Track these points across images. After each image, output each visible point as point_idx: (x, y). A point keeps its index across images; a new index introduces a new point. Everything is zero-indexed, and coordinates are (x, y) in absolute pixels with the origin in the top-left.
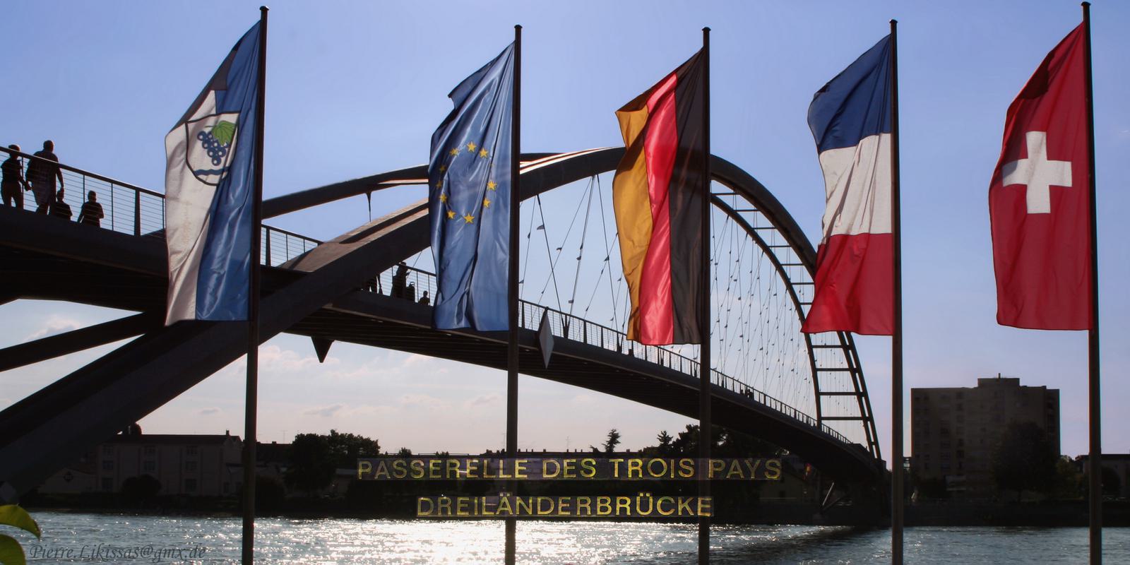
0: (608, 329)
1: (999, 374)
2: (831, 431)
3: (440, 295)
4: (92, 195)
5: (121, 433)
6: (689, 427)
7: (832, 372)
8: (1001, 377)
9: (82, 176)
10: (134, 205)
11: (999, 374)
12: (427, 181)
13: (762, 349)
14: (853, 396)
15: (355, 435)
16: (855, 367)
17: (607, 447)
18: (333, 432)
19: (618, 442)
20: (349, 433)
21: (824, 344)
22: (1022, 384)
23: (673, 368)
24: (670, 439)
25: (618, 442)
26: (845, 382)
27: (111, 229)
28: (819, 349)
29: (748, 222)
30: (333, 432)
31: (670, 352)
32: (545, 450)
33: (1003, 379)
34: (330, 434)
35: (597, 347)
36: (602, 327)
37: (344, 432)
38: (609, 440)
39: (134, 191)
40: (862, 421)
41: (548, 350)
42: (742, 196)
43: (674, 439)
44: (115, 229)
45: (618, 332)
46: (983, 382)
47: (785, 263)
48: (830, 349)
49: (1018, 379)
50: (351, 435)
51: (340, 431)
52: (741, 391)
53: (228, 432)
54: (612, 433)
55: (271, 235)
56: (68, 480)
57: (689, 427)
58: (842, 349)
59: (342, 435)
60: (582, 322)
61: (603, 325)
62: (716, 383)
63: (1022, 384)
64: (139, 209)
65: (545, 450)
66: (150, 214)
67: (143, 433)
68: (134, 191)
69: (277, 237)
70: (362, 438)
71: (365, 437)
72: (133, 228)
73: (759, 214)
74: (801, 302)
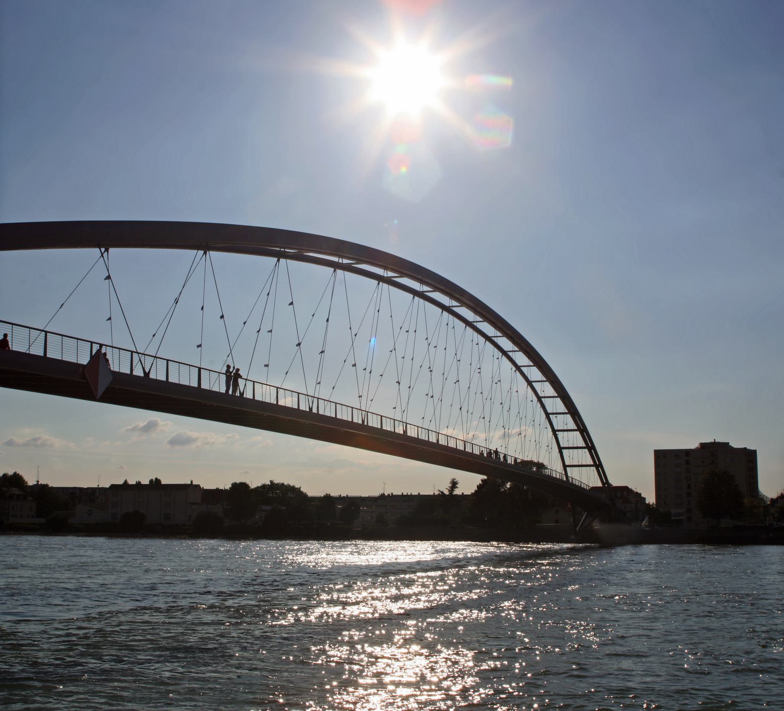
1: (715, 440)
2: (582, 484)
3: (311, 407)
4: (482, 451)
5: (508, 485)
6: (482, 480)
7: (572, 446)
8: (716, 441)
9: (178, 364)
10: (90, 350)
11: (715, 440)
12: (673, 518)
14: (592, 468)
15: (286, 484)
17: (449, 491)
18: (271, 482)
19: (457, 487)
25: (457, 487)
27: (61, 359)
28: (588, 463)
30: (271, 482)
32: (419, 494)
33: (717, 443)
34: (270, 484)
37: (278, 482)
38: (450, 486)
39: (130, 353)
40: (281, 259)
42: (523, 352)
44: (63, 359)
45: (403, 422)
46: (703, 445)
47: (544, 383)
48: (581, 450)
51: (276, 481)
52: (482, 454)
53: (402, 494)
54: (453, 481)
56: (90, 515)
57: (482, 480)
58: (578, 433)
62: (559, 478)
64: (201, 377)
65: (419, 494)
67: (162, 483)
68: (130, 353)
70: (290, 485)
71: (292, 485)
72: (43, 352)
73: (535, 368)
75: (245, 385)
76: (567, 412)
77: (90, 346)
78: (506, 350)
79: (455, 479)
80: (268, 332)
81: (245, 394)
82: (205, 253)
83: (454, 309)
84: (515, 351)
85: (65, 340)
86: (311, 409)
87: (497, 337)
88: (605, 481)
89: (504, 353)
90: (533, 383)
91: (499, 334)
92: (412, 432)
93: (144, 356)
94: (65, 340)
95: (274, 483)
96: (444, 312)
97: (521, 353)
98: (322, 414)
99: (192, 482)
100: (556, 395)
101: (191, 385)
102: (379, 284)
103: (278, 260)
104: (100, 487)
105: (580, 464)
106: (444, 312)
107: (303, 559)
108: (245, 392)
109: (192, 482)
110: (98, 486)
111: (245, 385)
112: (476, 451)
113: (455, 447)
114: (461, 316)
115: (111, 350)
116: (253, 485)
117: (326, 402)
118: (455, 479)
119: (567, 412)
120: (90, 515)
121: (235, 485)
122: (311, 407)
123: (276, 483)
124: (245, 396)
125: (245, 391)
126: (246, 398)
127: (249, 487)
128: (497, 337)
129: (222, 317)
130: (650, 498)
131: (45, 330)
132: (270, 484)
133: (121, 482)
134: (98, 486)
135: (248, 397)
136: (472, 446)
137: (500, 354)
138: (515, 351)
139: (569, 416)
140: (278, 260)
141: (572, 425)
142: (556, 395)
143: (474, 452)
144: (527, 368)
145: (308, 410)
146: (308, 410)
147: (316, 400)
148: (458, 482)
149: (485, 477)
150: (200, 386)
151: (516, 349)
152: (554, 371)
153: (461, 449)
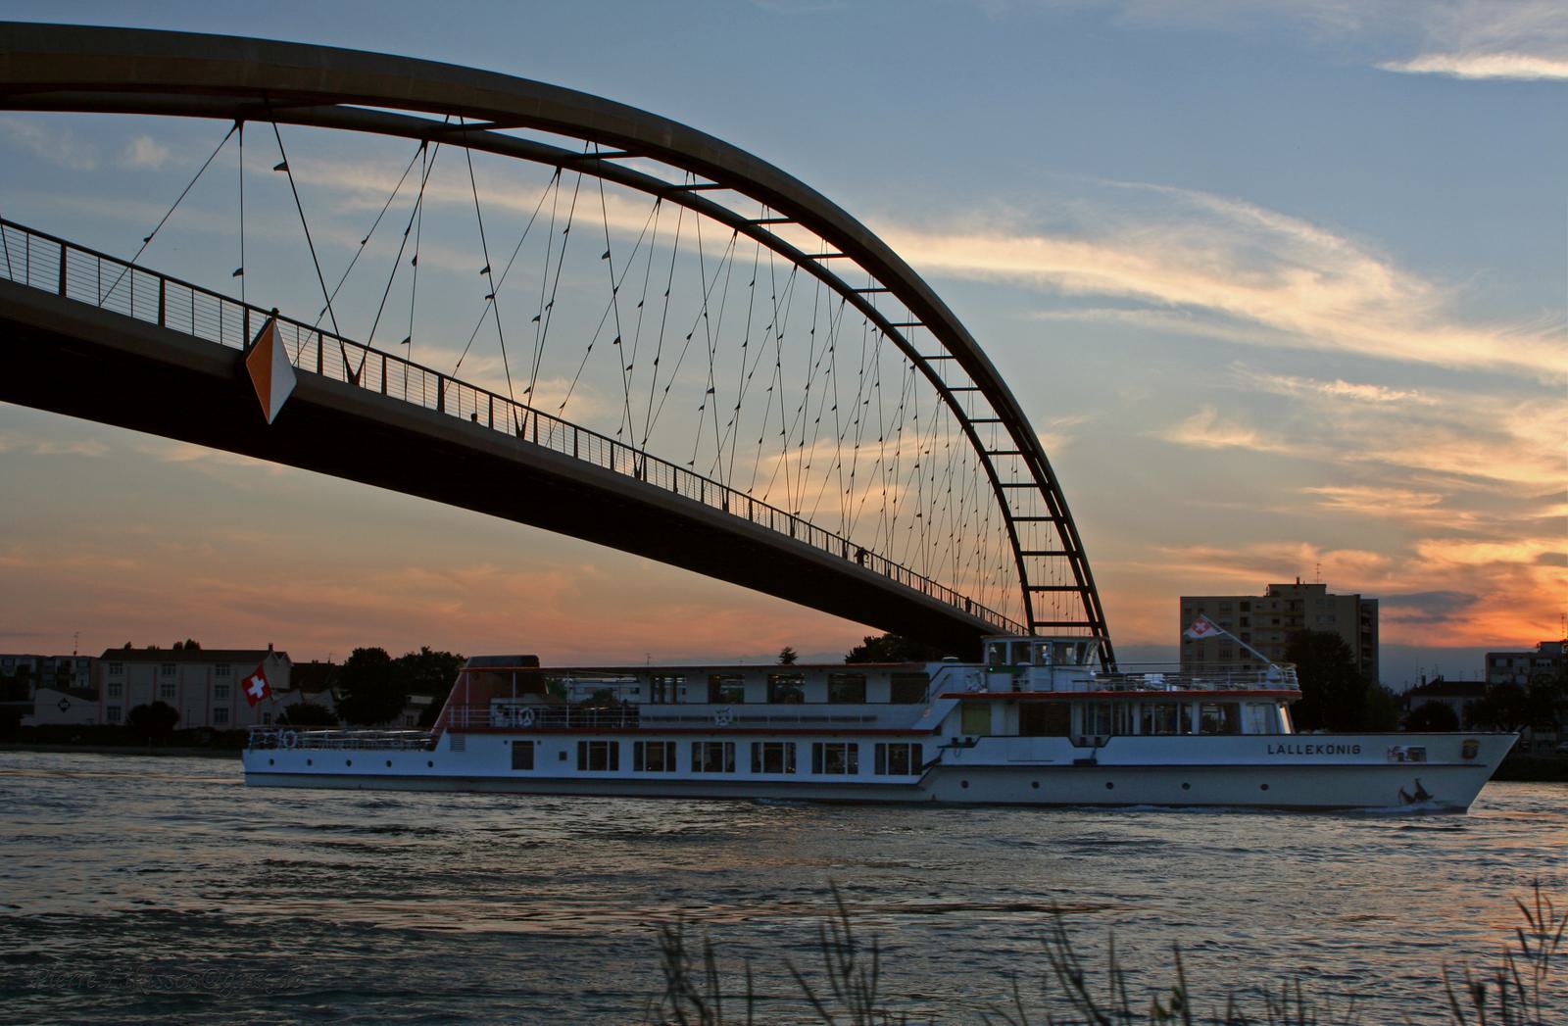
0: (816, 528)
7: (1057, 584)
13: (920, 515)
16: (1097, 620)
18: (424, 650)
20: (445, 652)
21: (993, 450)
22: (1328, 591)
23: (541, 442)
24: (37, 688)
26: (1062, 570)
29: (961, 405)
30: (424, 650)
31: (613, 442)
34: (421, 653)
35: (423, 409)
36: (676, 467)
39: (159, 279)
41: (277, 397)
43: (32, 692)
45: (635, 451)
50: (448, 654)
51: (434, 649)
55: (166, 286)
56: (64, 710)
57: (868, 640)
59: (436, 654)
60: (825, 534)
61: (774, 506)
63: (1328, 591)
66: (145, 306)
69: (140, 277)
74: (970, 418)
75: (364, 361)
76: (1018, 450)
77: (159, 284)
78: (923, 354)
79: (790, 650)
80: (482, 273)
81: (362, 379)
82: (239, 125)
83: (823, 262)
84: (945, 358)
85: (227, 307)
86: (521, 433)
87: (908, 325)
88: (1107, 656)
89: (888, 329)
91: (833, 249)
92: (658, 478)
93: (130, 269)
94: (227, 307)
95: (430, 652)
96: (846, 301)
97: (954, 361)
98: (544, 445)
99: (271, 646)
100: (998, 418)
101: (137, 315)
102: (659, 202)
103: (558, 172)
104: (78, 655)
105: (1063, 584)
106: (846, 301)
107: (1542, 515)
108: (362, 375)
109: (271, 646)
110: (75, 653)
111: (364, 361)
112: (820, 540)
113: (769, 526)
114: (731, 172)
115: (219, 304)
116: (395, 653)
117: (553, 422)
118: (790, 650)
119: (1018, 450)
120: (64, 710)
121: (359, 654)
122: (520, 426)
123: (433, 652)
124: (362, 384)
125: (363, 371)
126: (365, 389)
127: (388, 658)
128: (908, 325)
129: (618, 341)
130: (176, 727)
131: (318, 327)
132: (864, 645)
133: (121, 646)
134: (75, 653)
135: (368, 387)
136: (844, 545)
137: (838, 297)
138: (945, 358)
139: (1020, 457)
140: (558, 172)
141: (1026, 475)
142: (998, 418)
143: (831, 551)
144: (906, 328)
145: (513, 433)
146: (513, 433)
147: (531, 415)
148: (796, 655)
149: (878, 633)
150: (65, 294)
151: (917, 320)
152: (1016, 397)
153: (783, 531)
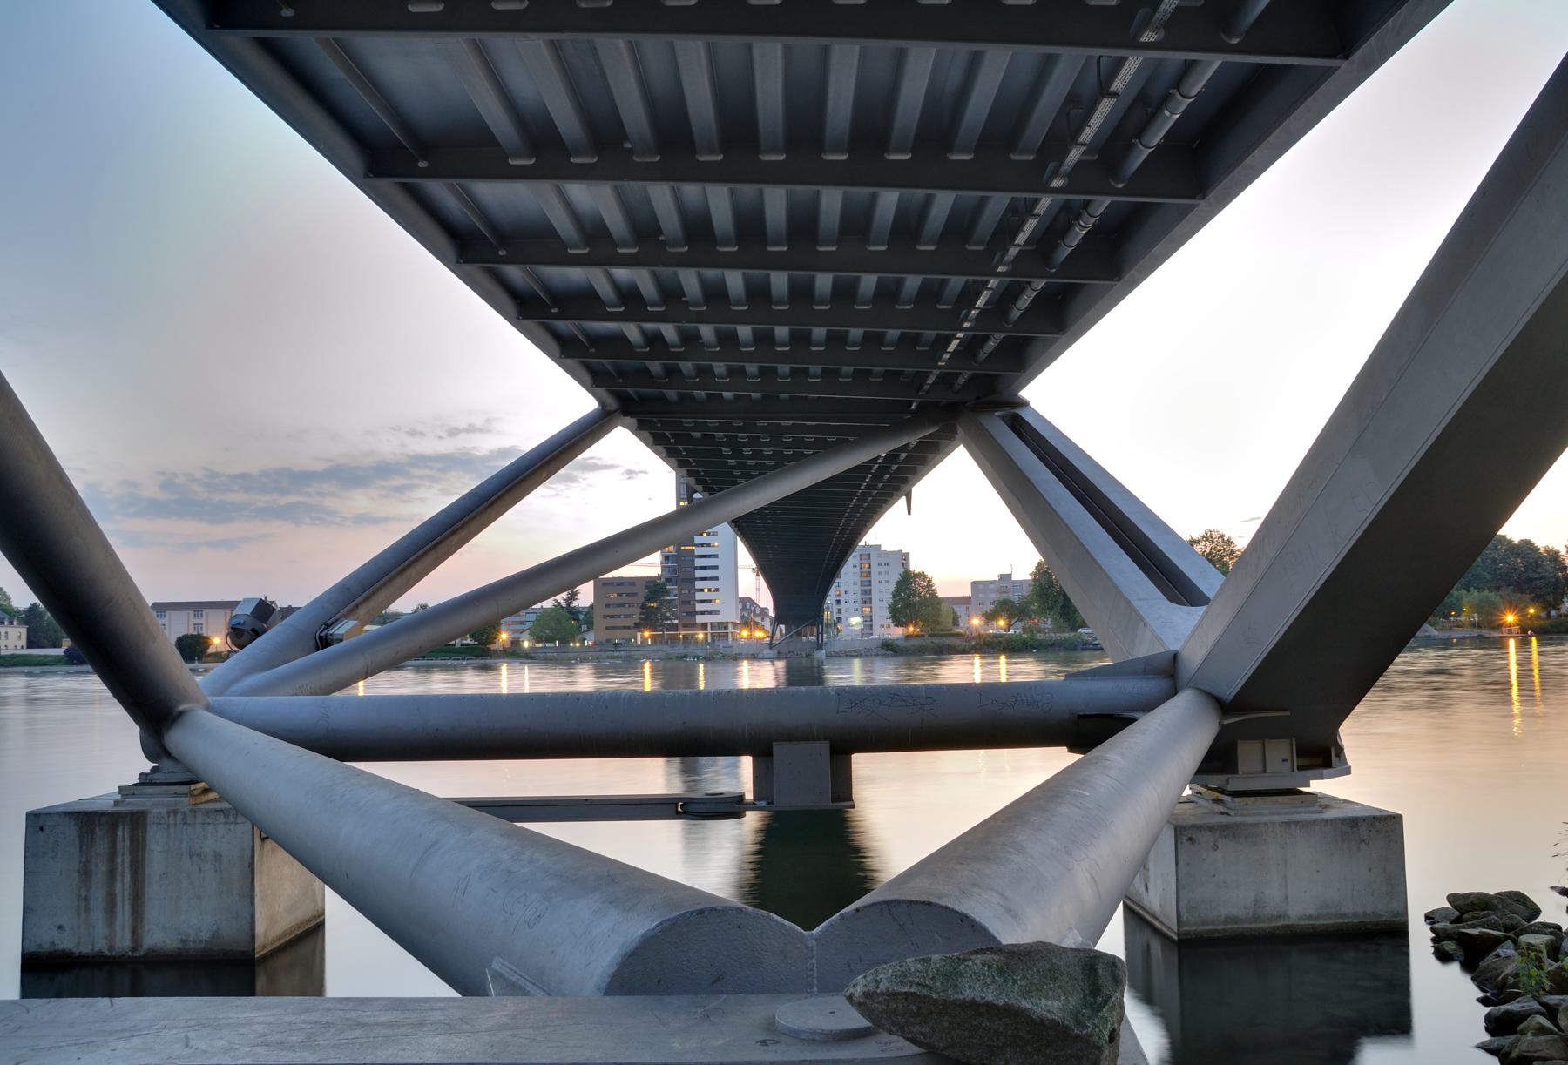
22: (882, 549)
49: (880, 546)
63: (882, 549)
90: (904, 499)
130: (210, 651)
